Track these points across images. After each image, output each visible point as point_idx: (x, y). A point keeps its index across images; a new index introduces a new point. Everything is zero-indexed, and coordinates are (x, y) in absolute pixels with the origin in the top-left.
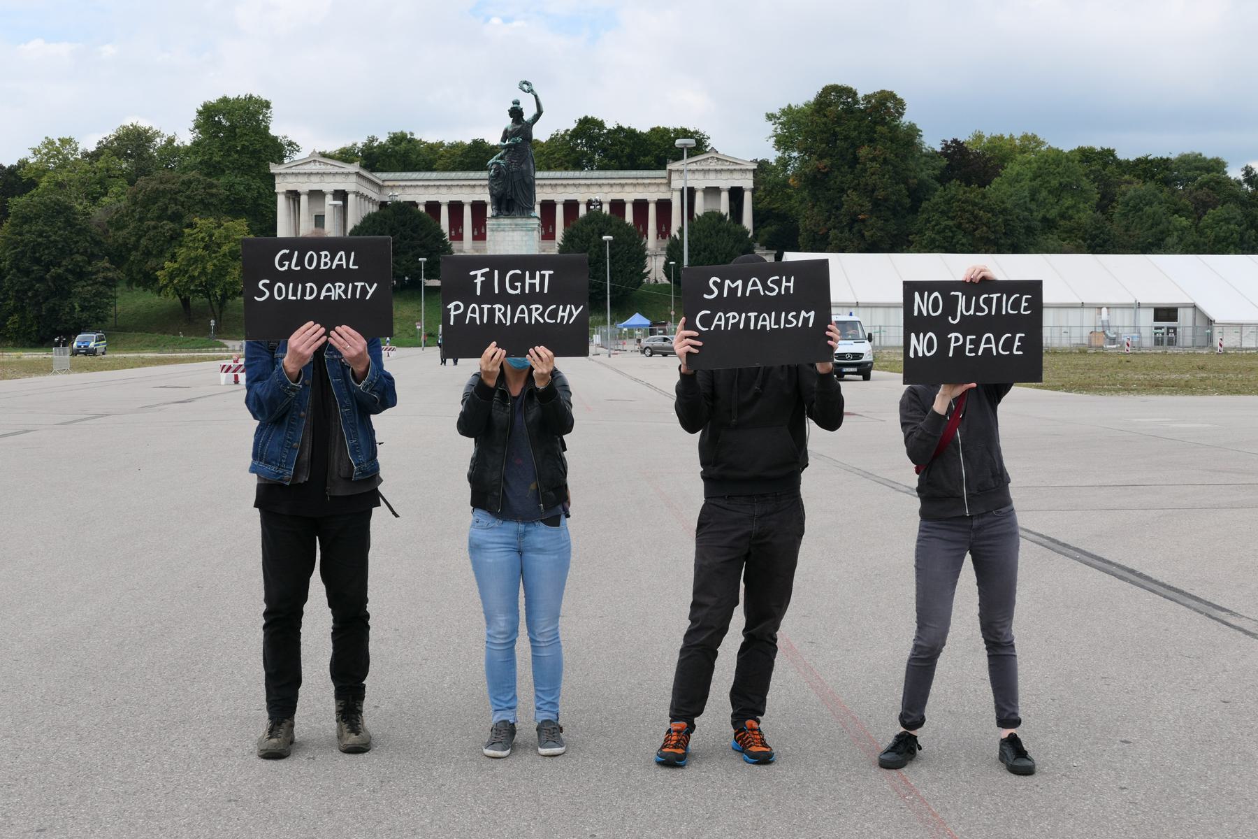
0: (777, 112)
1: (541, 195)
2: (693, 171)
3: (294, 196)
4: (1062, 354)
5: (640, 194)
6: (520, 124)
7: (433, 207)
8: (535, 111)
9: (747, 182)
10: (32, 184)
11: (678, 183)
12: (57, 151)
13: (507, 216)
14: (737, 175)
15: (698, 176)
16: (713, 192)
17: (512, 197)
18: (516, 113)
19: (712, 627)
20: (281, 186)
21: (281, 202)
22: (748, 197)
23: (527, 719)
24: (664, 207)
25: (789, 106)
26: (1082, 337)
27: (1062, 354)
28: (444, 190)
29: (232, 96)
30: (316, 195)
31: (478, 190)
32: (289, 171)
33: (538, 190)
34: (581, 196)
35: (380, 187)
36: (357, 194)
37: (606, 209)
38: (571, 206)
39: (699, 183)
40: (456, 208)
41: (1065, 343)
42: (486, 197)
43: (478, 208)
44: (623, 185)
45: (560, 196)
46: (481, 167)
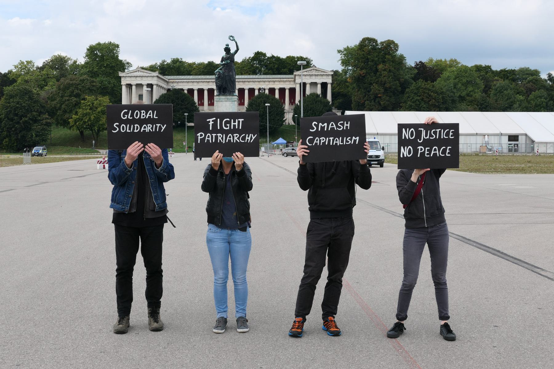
0: (342, 49)
1: (238, 86)
2: (305, 75)
3: (129, 86)
4: (468, 155)
5: (282, 85)
6: (229, 55)
7: (191, 91)
8: (236, 49)
9: (329, 80)
10: (14, 81)
11: (298, 80)
12: (25, 67)
13: (223, 95)
14: (324, 77)
15: (307, 77)
16: (314, 84)
17: (225, 87)
18: (227, 50)
20: (124, 82)
21: (124, 89)
22: (329, 87)
23: (232, 316)
24: (292, 91)
25: (348, 47)
26: (476, 148)
27: (468, 155)
28: (195, 84)
29: (102, 42)
30: (139, 86)
31: (211, 84)
32: (127, 75)
33: (237, 83)
34: (256, 86)
35: (168, 82)
36: (157, 85)
37: (267, 92)
38: (252, 91)
39: (308, 80)
40: (201, 91)
41: (469, 151)
42: (214, 87)
43: (211, 91)
44: (274, 82)
45: (247, 86)
46: (212, 73)
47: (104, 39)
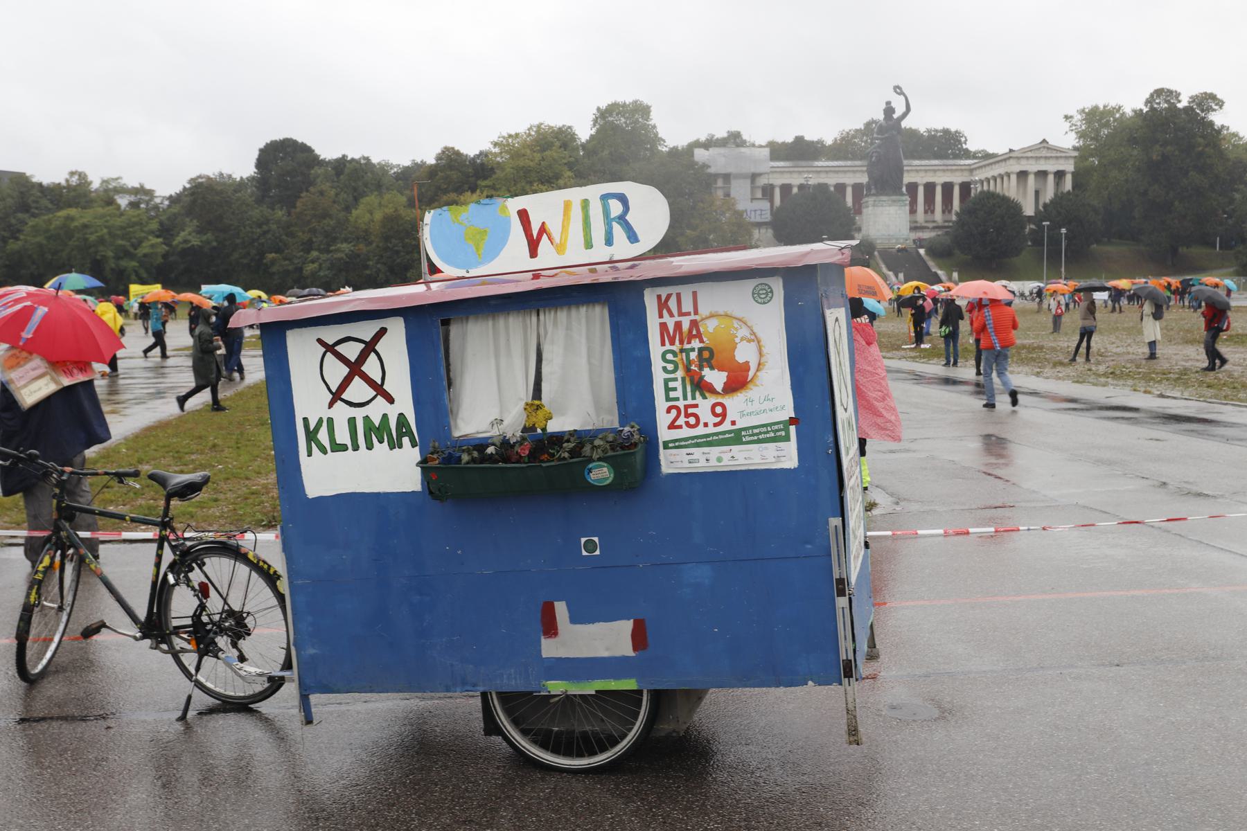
1: (907, 179)
7: (841, 188)
8: (904, 109)
14: (1062, 161)
15: (1031, 161)
16: (1042, 174)
17: (886, 181)
18: (889, 110)
19: (198, 669)
25: (598, 109)
26: (569, 328)
28: (795, 175)
31: (858, 175)
33: (905, 175)
37: (795, 190)
43: (857, 188)
44: (935, 171)
45: (921, 179)
47: (626, 97)
